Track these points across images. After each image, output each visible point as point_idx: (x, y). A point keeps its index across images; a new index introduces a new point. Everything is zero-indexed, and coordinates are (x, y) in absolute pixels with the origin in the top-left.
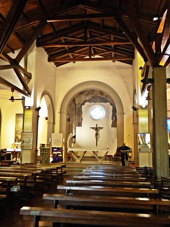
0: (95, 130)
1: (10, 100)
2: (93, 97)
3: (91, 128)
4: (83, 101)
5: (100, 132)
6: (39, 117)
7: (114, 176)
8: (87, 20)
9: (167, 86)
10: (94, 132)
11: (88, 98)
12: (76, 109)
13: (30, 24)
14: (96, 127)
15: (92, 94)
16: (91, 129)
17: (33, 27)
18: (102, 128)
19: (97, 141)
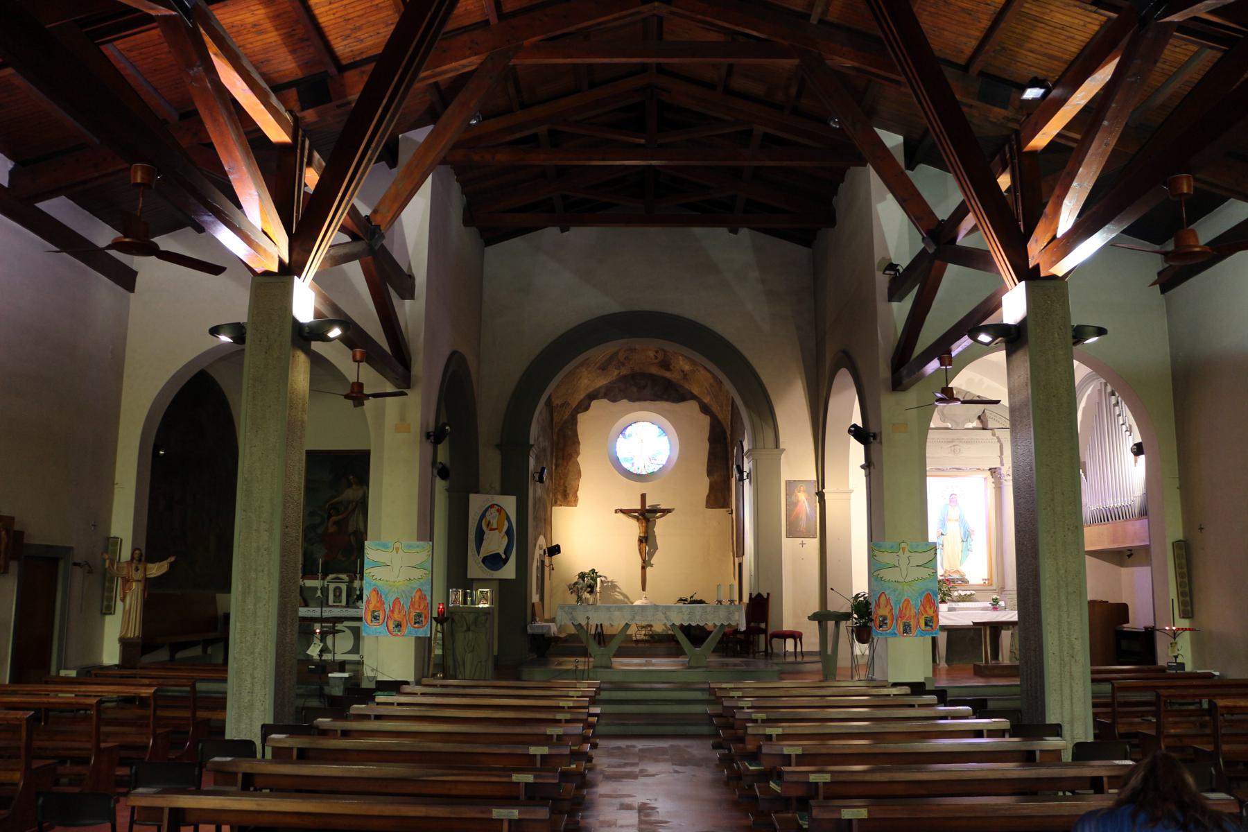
0: (638, 519)
1: (347, 397)
2: (625, 376)
3: (616, 511)
4: (581, 395)
5: (661, 527)
6: (852, 495)
7: (68, 681)
8: (659, 65)
9: (100, 275)
10: (633, 528)
11: (602, 382)
12: (552, 429)
13: (438, 70)
14: (639, 507)
15: (623, 364)
16: (620, 515)
17: (436, 84)
18: (666, 512)
19: (643, 568)
